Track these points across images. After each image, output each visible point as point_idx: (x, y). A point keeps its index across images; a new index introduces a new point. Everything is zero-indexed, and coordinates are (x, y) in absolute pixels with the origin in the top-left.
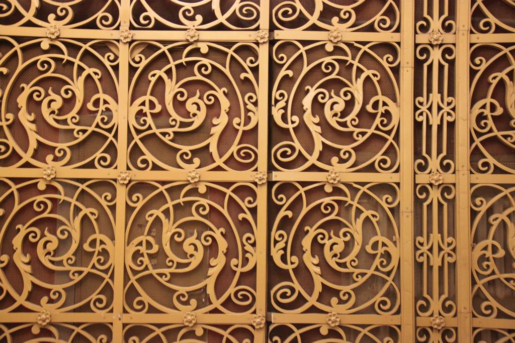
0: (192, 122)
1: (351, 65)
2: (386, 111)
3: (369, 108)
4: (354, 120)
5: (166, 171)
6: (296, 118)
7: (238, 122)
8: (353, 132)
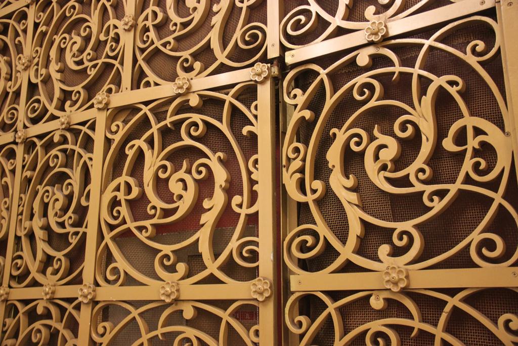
0: (176, 209)
1: (408, 77)
2: (483, 144)
3: (448, 144)
4: (422, 170)
5: (146, 287)
6: (318, 185)
7: (239, 202)
8: (422, 193)
